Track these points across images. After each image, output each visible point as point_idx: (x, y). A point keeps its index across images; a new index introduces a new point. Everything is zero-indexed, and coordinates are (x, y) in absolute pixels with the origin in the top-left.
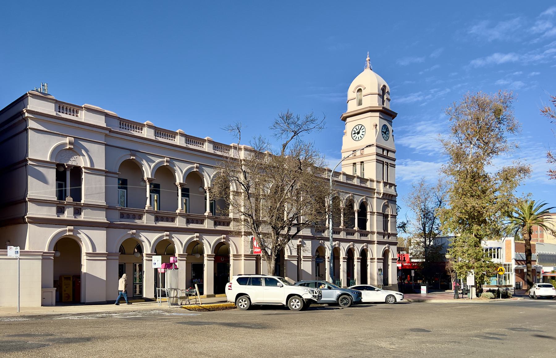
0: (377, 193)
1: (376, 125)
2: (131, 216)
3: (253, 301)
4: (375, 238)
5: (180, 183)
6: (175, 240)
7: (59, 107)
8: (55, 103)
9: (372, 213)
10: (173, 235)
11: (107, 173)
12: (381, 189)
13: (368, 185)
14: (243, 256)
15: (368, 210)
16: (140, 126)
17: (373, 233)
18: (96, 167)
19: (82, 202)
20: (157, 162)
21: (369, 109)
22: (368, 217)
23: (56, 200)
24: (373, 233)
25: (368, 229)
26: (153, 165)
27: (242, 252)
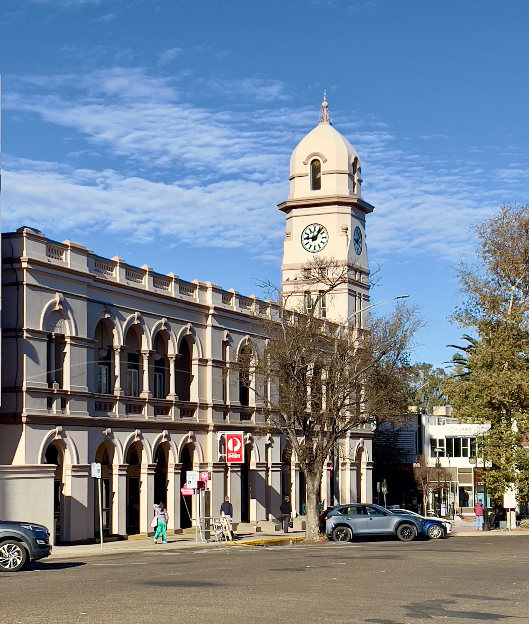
1: (347, 229)
4: (209, 418)
8: (46, 243)
9: (203, 362)
10: (67, 432)
15: (195, 355)
17: (204, 406)
18: (80, 336)
20: (128, 319)
21: (336, 200)
22: (195, 370)
23: (240, 405)
24: (204, 406)
25: (194, 398)
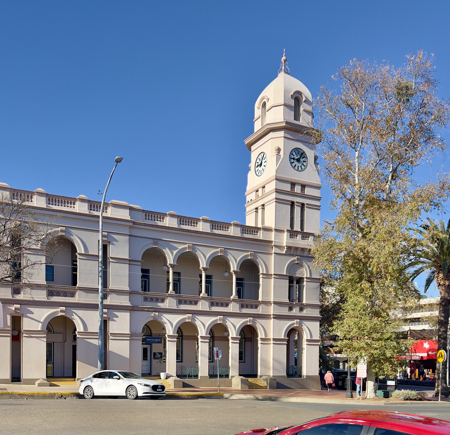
0: (275, 246)
1: (279, 150)
2: (154, 299)
3: (95, 395)
5: (234, 271)
6: (198, 323)
7: (146, 215)
9: (267, 276)
11: (131, 262)
12: (285, 240)
13: (261, 235)
14: (272, 339)
16: (162, 216)
17: (267, 303)
19: (77, 285)
23: (46, 284)
24: (267, 303)
26: (175, 252)
27: (271, 336)
